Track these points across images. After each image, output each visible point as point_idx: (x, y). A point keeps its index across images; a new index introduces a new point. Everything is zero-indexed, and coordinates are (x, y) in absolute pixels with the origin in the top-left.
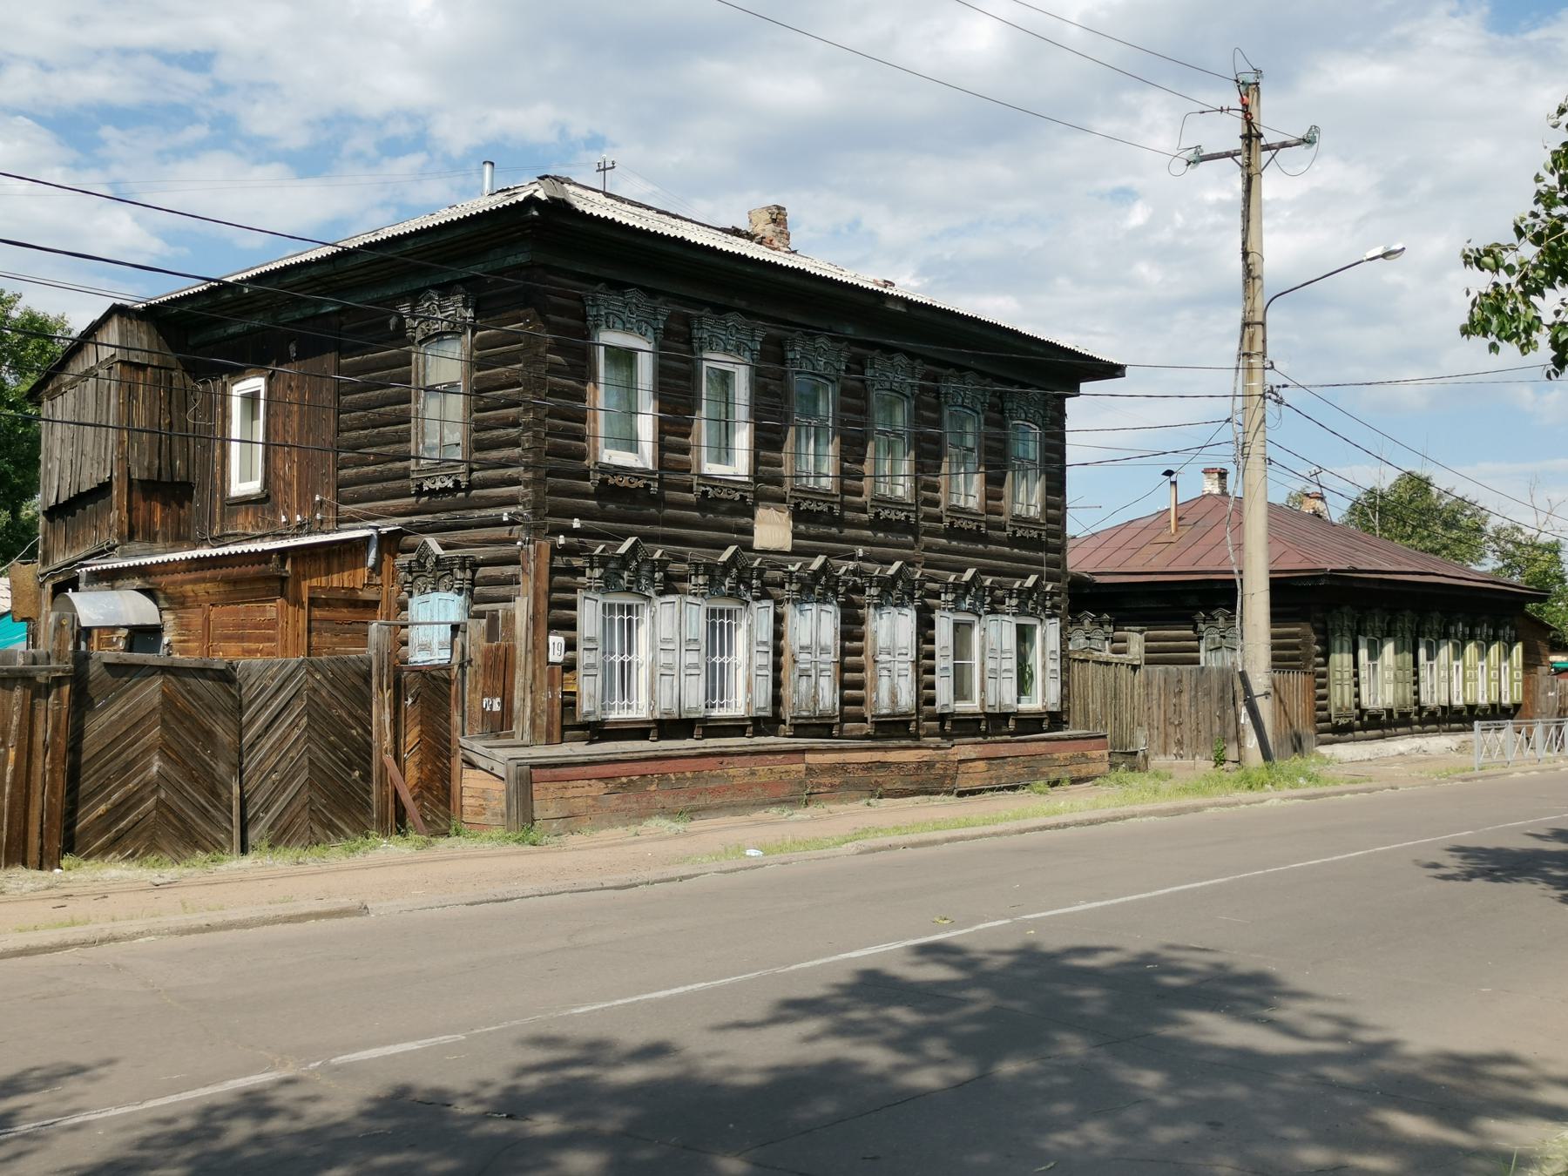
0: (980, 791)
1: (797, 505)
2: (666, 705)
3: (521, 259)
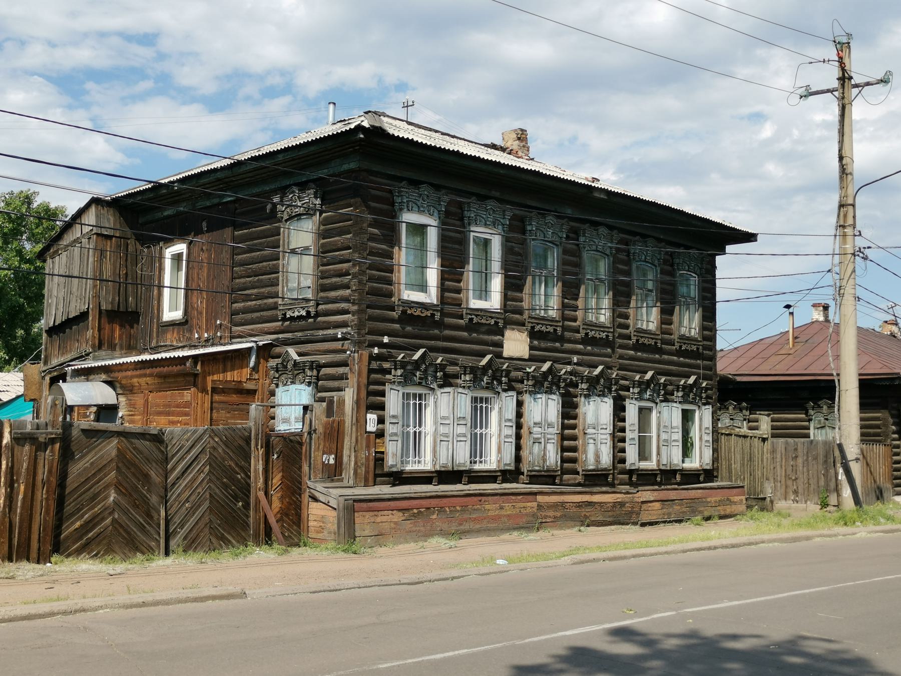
0: (656, 523)
1: (533, 328)
2: (444, 461)
3: (353, 165)
